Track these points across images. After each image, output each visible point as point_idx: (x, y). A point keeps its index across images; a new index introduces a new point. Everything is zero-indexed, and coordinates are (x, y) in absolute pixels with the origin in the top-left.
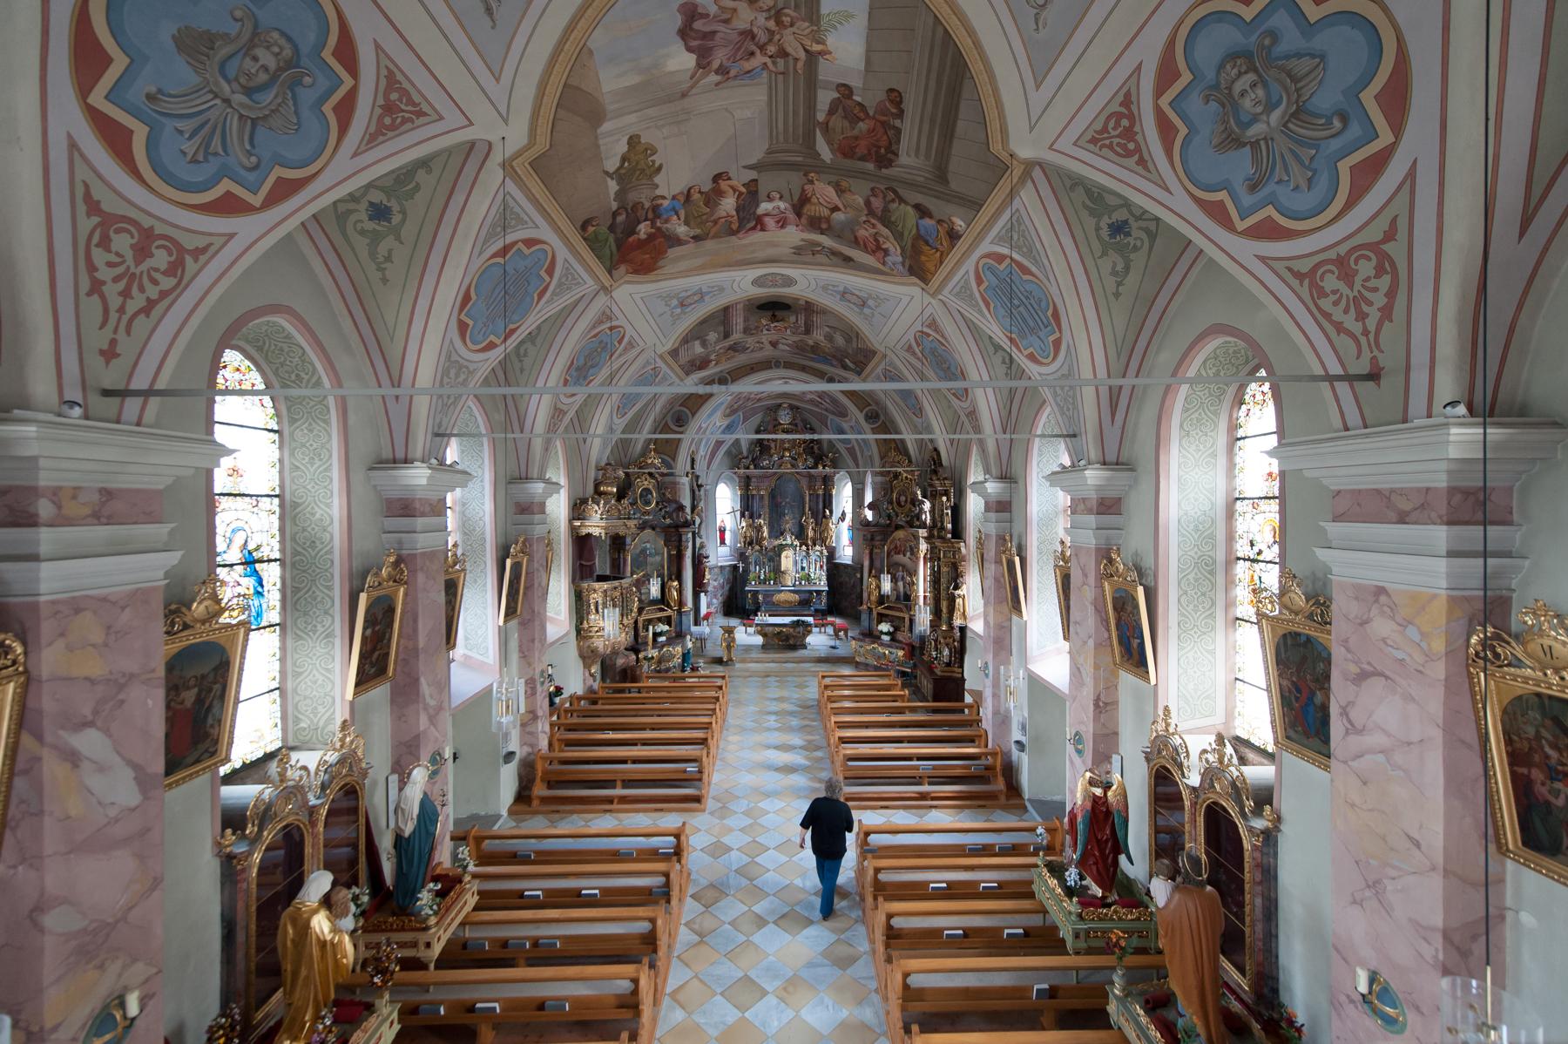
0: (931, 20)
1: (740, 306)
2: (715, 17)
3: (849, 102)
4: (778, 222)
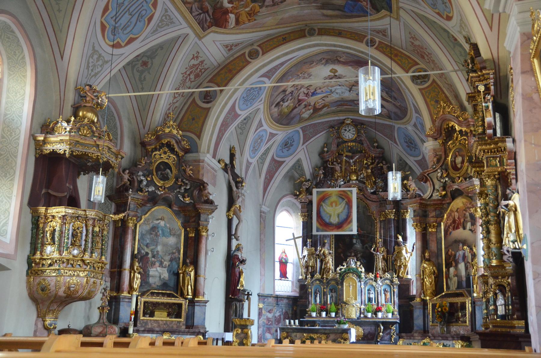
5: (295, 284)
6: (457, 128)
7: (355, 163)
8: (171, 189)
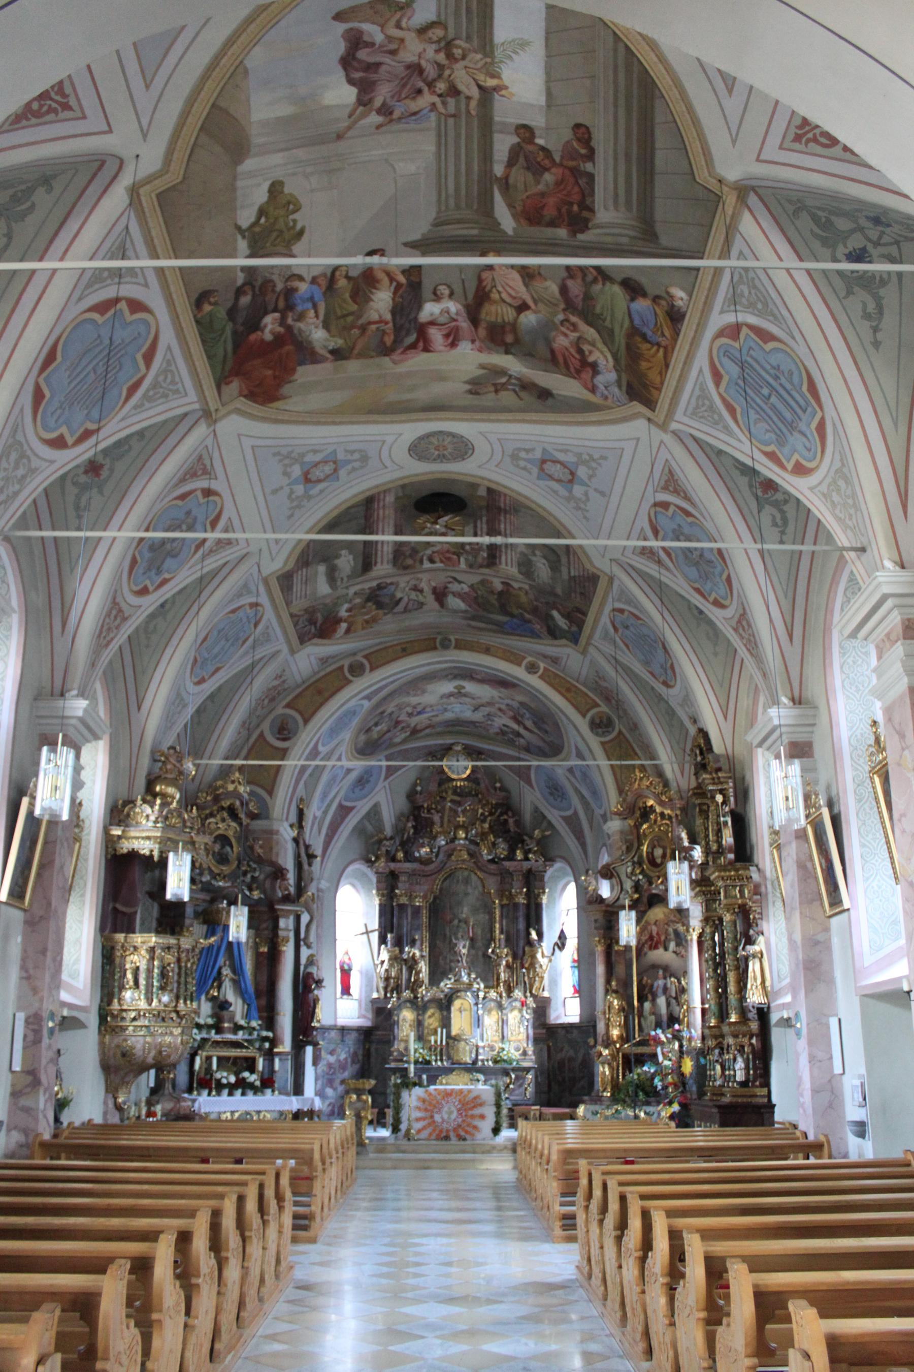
0: (611, 39)
1: (390, 499)
2: (381, 46)
3: (531, 148)
4: (447, 336)
5: (363, 1005)
6: (658, 809)
7: (464, 811)
8: (233, 877)
